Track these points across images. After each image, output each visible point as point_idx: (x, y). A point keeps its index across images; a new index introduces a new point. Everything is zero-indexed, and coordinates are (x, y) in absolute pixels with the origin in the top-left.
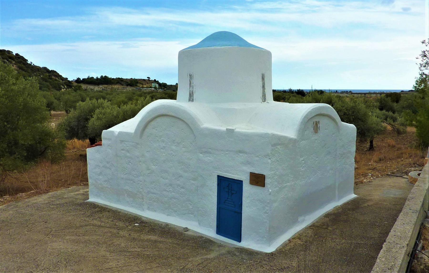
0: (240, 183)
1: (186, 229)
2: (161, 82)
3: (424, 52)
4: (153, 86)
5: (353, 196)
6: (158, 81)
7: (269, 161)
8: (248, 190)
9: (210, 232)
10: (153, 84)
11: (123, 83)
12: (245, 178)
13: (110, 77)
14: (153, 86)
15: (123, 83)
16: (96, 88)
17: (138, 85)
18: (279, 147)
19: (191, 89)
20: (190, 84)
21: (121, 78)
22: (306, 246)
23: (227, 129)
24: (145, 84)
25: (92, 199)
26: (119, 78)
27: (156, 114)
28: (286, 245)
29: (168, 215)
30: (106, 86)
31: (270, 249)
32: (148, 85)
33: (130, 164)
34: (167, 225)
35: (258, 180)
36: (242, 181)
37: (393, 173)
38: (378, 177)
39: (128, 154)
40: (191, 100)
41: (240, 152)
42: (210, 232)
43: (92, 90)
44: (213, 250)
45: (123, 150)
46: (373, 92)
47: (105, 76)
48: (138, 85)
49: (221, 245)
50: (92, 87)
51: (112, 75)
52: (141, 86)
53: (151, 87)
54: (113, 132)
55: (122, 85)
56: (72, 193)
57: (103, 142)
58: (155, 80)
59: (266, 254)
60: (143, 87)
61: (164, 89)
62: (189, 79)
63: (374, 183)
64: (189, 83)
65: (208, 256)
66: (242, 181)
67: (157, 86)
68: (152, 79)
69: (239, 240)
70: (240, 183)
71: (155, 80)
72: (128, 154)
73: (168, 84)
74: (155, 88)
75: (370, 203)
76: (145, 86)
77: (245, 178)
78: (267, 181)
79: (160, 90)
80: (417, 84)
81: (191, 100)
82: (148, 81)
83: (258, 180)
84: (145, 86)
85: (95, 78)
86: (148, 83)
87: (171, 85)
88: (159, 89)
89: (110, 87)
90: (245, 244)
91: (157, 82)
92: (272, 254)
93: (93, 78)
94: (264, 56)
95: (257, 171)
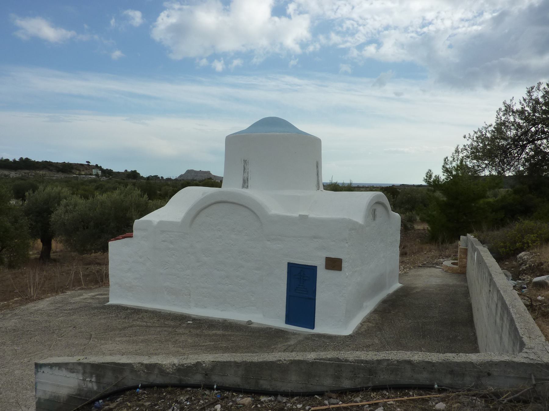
0: (313, 270)
1: (250, 322)
2: (104, 167)
3: (464, 146)
4: (94, 173)
5: (398, 285)
6: (101, 167)
7: (347, 245)
8: (323, 276)
9: (277, 321)
10: (94, 170)
11: (51, 168)
13: (33, 160)
14: (94, 173)
15: (51, 168)
16: (13, 174)
17: (73, 171)
18: (353, 231)
19: (246, 175)
21: (50, 162)
22: (378, 327)
23: (300, 215)
24: (83, 170)
25: (113, 301)
26: (46, 162)
27: (213, 201)
28: (360, 328)
29: (222, 311)
30: (27, 171)
31: (348, 331)
32: (87, 172)
33: (174, 256)
34: (225, 320)
35: (334, 264)
36: (316, 267)
37: (424, 264)
38: (410, 269)
39: (172, 246)
40: (246, 186)
41: (315, 237)
42: (277, 321)
43: (6, 176)
44: (290, 338)
45: (164, 241)
46: (361, 186)
47: (27, 159)
48: (73, 171)
49: (294, 334)
50: (6, 172)
51: (37, 157)
52: (78, 172)
53: (91, 174)
54: (150, 222)
55: (51, 171)
56: (87, 296)
57: (135, 233)
58: (97, 165)
59: (345, 336)
60: (80, 174)
61: (109, 177)
62: (243, 164)
63: (410, 274)
64: (243, 168)
65: (289, 343)
66: (316, 267)
67: (100, 172)
68: (93, 163)
69: (313, 328)
70: (313, 270)
71: (97, 165)
72: (172, 246)
73: (115, 170)
74: (97, 175)
75: (418, 290)
76: (83, 173)
78: (344, 265)
79: (104, 178)
80: (427, 176)
81: (246, 186)
82: (88, 167)
83: (334, 264)
84: (83, 173)
85: (17, 160)
86: (87, 169)
87: (118, 173)
88: (102, 176)
89: (33, 173)
90: (320, 328)
91: (100, 168)
92: (351, 336)
93: (8, 160)
94: (312, 145)
95: (333, 255)
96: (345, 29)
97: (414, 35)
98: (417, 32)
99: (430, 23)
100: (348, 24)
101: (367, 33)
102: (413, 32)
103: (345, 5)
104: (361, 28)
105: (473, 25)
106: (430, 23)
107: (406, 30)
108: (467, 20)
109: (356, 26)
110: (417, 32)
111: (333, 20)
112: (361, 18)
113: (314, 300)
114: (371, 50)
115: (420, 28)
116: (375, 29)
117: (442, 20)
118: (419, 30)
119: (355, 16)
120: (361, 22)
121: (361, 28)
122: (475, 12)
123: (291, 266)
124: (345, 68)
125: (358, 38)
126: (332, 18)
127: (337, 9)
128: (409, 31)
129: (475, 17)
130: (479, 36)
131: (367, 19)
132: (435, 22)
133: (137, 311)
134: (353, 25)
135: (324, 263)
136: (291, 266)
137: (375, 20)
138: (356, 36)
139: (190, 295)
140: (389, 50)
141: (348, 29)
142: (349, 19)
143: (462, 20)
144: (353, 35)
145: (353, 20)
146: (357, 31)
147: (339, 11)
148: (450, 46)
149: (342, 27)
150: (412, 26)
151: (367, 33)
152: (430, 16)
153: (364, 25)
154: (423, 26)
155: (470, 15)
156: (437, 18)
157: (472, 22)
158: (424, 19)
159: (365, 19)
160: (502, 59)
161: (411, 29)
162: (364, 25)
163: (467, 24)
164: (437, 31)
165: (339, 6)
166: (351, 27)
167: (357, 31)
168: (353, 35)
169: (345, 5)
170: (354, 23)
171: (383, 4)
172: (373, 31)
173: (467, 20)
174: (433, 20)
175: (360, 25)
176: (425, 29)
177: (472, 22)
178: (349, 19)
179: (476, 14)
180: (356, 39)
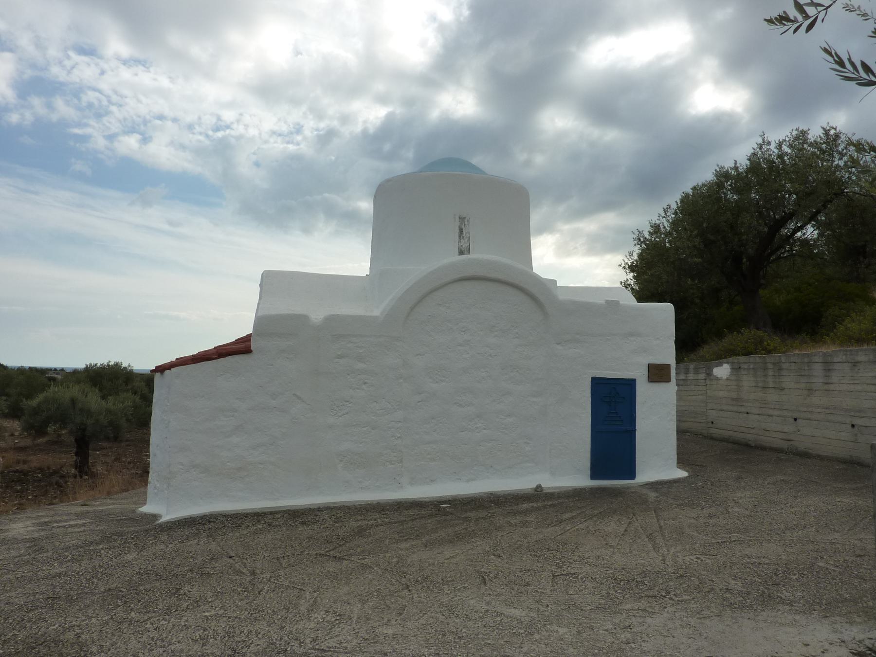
0: (630, 384)
12: (640, 374)
20: (461, 232)
29: (468, 481)
33: (364, 387)
36: (634, 380)
39: (361, 366)
45: (340, 357)
62: (457, 223)
64: (458, 231)
66: (634, 380)
70: (630, 384)
72: (361, 366)
77: (640, 374)
96: (84, 104)
97: (201, 138)
98: (207, 136)
99: (228, 127)
100: (92, 96)
101: (125, 119)
102: (201, 134)
103: (89, 65)
104: (114, 109)
105: (288, 143)
106: (228, 127)
107: (190, 127)
108: (280, 135)
109: (105, 102)
110: (207, 136)
111: (62, 84)
112: (116, 92)
113: (634, 431)
114: (130, 144)
115: (213, 131)
116: (139, 117)
117: (246, 126)
118: (210, 133)
119: (104, 86)
120: (115, 98)
121: (114, 109)
122: (292, 126)
123: (597, 383)
124: (78, 166)
125: (107, 124)
126: (61, 79)
127: (73, 67)
128: (195, 131)
129: (292, 133)
130: (297, 158)
131: (126, 97)
132: (235, 126)
133: (258, 516)
134: (100, 101)
135: (646, 373)
136: (597, 383)
137: (139, 101)
138: (105, 119)
139: (401, 461)
140: (162, 152)
141: (90, 105)
142: (95, 89)
143: (273, 133)
144: (99, 116)
145: (100, 92)
146: (108, 113)
147: (75, 70)
148: (257, 164)
149: (79, 99)
150: (200, 125)
151: (125, 119)
152: (229, 116)
153: (121, 106)
154: (217, 129)
155: (284, 129)
156: (238, 121)
157: (287, 139)
158: (219, 118)
159: (122, 96)
160: (327, 195)
161: (198, 129)
162: (121, 106)
163: (279, 139)
164: (239, 138)
165: (77, 64)
166: (96, 103)
167: (108, 113)
168: (99, 116)
169: (89, 65)
170: (103, 98)
171: (155, 79)
172: (135, 117)
173: (280, 135)
174: (232, 123)
175: (113, 104)
176: (220, 134)
177: (287, 139)
178: (95, 89)
179: (293, 130)
180: (104, 125)
